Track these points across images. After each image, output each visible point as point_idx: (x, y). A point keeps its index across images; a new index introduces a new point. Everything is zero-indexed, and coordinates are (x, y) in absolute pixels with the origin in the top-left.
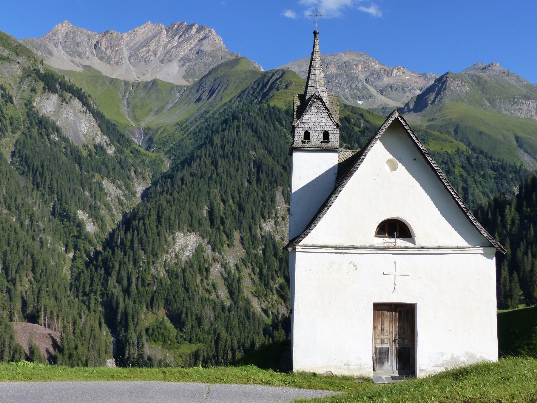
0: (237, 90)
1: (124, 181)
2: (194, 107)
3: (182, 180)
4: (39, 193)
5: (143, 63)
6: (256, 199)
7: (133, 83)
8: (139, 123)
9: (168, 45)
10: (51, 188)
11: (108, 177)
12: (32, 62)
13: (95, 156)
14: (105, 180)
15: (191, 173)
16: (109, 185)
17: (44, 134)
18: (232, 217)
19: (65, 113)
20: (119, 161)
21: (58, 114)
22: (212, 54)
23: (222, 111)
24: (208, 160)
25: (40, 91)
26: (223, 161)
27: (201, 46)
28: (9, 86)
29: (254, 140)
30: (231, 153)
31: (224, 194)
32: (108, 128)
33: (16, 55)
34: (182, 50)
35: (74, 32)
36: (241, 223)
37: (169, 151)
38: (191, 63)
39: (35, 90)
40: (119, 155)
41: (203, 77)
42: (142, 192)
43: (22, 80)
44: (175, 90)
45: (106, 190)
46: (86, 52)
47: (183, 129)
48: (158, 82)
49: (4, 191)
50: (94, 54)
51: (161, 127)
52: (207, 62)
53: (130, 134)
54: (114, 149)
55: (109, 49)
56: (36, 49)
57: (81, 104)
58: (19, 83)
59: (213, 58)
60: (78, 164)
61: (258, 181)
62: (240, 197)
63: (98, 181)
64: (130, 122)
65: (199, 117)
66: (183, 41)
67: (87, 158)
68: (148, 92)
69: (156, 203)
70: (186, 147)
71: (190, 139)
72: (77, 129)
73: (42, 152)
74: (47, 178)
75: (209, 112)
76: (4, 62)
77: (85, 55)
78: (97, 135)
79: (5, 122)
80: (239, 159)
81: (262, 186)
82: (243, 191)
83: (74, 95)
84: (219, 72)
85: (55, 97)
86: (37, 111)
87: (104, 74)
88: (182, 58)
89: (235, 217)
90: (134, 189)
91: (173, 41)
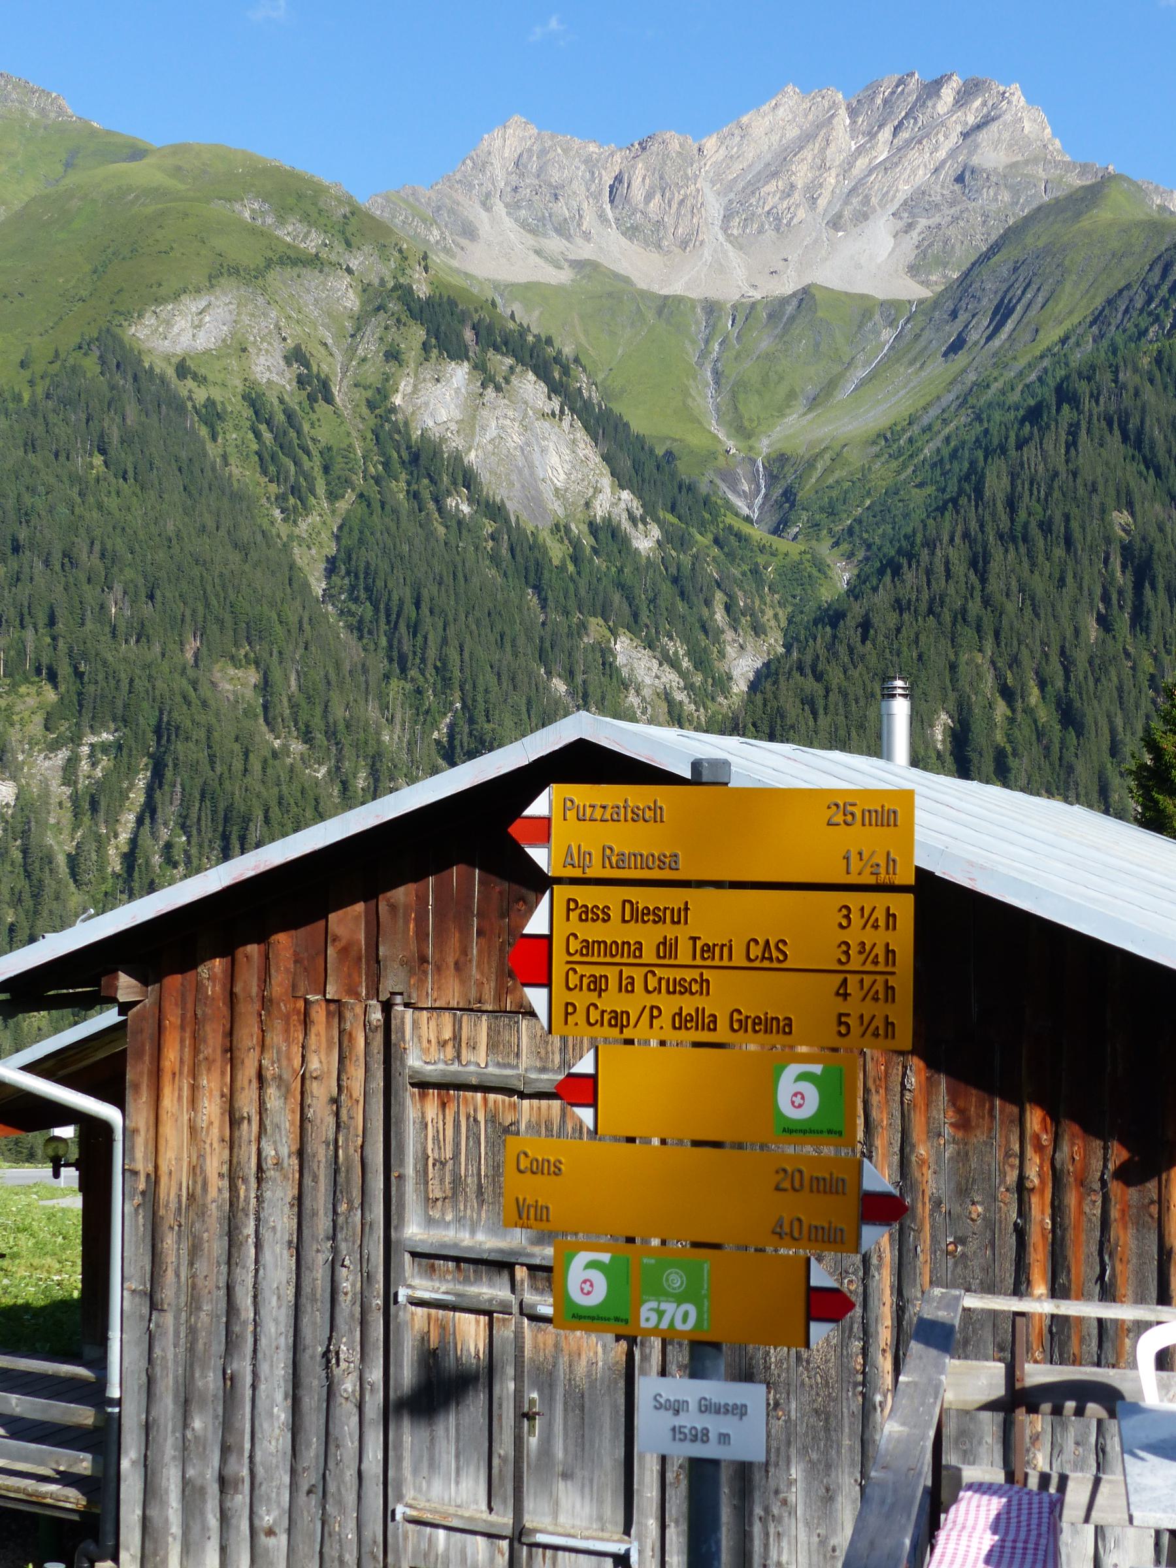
0: (1093, 297)
1: (686, 640)
2: (938, 370)
3: (865, 626)
4: (409, 686)
5: (770, 234)
6: (1128, 684)
7: (735, 307)
8: (751, 442)
9: (858, 163)
10: (442, 670)
11: (634, 625)
12: (392, 264)
13: (591, 561)
14: (623, 638)
15: (898, 601)
16: (635, 654)
17: (426, 495)
18: (1036, 750)
19: (493, 424)
20: (675, 572)
21: (473, 427)
22: (1011, 178)
23: (1033, 377)
24: (958, 555)
25: (412, 354)
26: (1012, 555)
27: (971, 154)
28: (322, 349)
29: (1131, 473)
30: (1041, 525)
31: (1010, 667)
32: (637, 467)
33: (344, 246)
34: (906, 175)
35: (543, 152)
36: (1070, 769)
37: (850, 531)
38: (937, 219)
39: (398, 352)
40: (674, 554)
41: (973, 264)
42: (751, 676)
43: (360, 322)
44: (877, 317)
45: (625, 672)
46: (581, 217)
47: (900, 452)
48: (818, 296)
49: (293, 683)
50: (607, 220)
51: (826, 449)
52: (994, 207)
53: (718, 481)
54: (656, 532)
55: (658, 196)
56: (424, 221)
57: (543, 388)
58: (352, 336)
59: (1016, 191)
60: (535, 587)
61: (1140, 618)
62: (1067, 678)
63: (600, 643)
64: (720, 441)
65: (952, 409)
66: (908, 143)
67: (562, 568)
68: (786, 330)
69: (765, 705)
70: (906, 516)
71: (921, 485)
72: (532, 474)
73: (416, 556)
74: (431, 637)
75: (988, 386)
76: (304, 271)
77: (579, 225)
78: (597, 490)
79: (306, 464)
80: (1069, 542)
81: (1153, 637)
82: (1081, 657)
83: (520, 360)
84: (1029, 240)
85: (459, 374)
86: (406, 424)
87: (642, 285)
88: (905, 203)
89: (1047, 748)
90: (721, 667)
91: (872, 148)
